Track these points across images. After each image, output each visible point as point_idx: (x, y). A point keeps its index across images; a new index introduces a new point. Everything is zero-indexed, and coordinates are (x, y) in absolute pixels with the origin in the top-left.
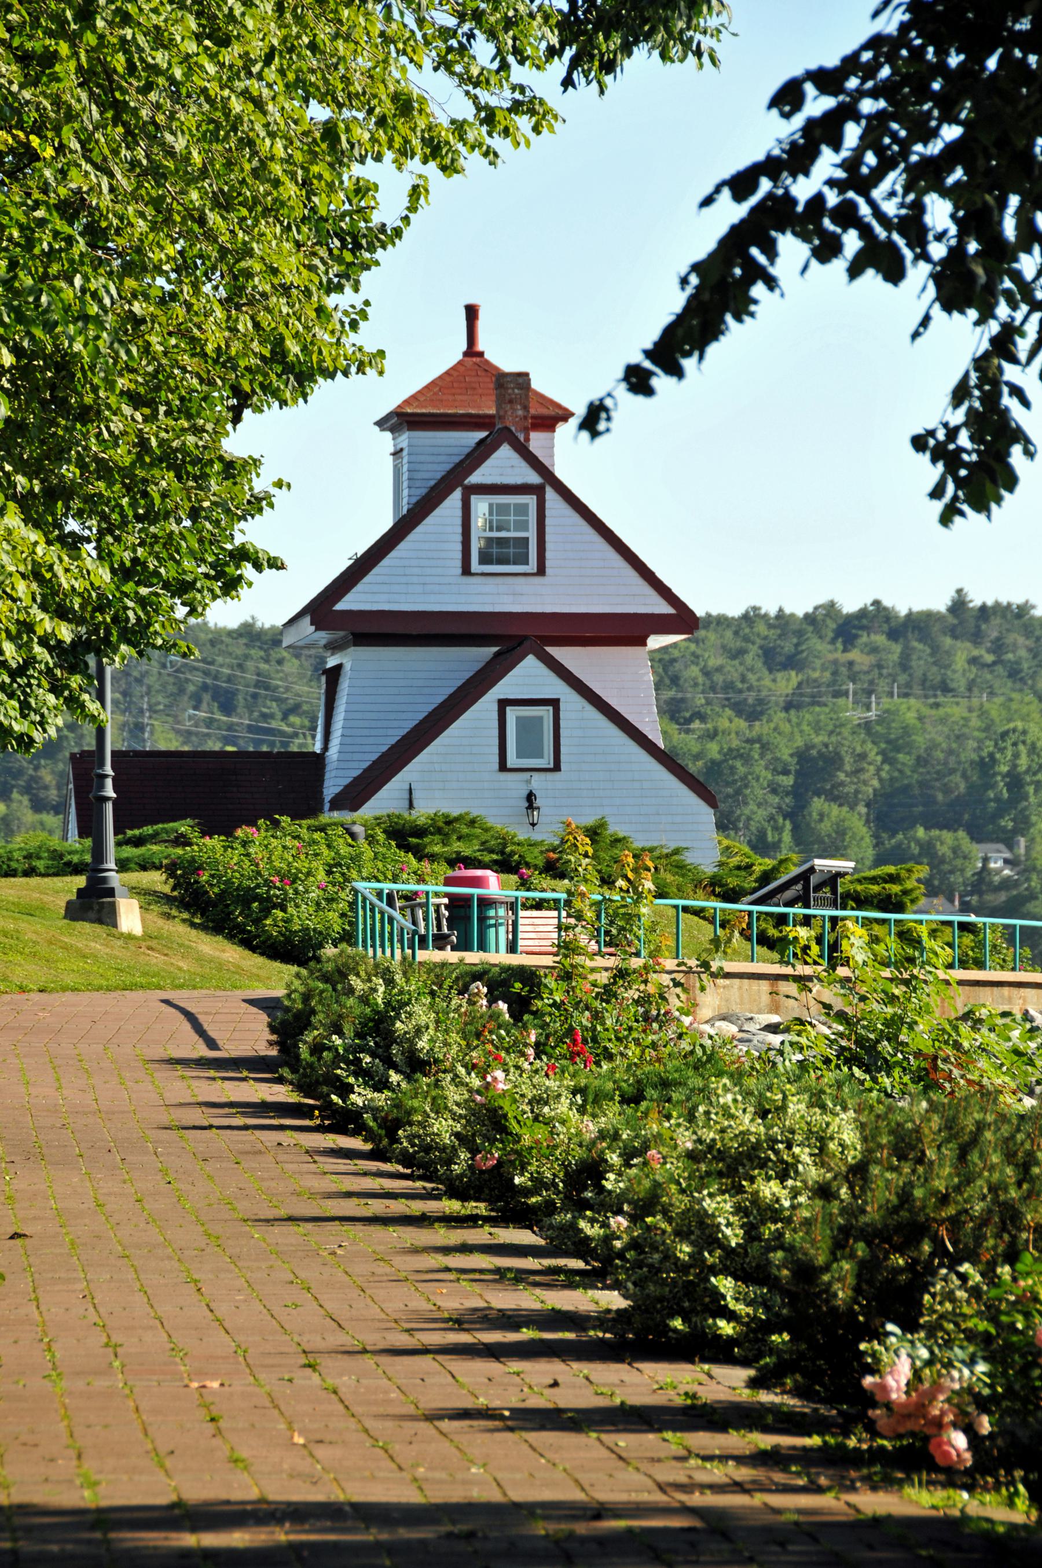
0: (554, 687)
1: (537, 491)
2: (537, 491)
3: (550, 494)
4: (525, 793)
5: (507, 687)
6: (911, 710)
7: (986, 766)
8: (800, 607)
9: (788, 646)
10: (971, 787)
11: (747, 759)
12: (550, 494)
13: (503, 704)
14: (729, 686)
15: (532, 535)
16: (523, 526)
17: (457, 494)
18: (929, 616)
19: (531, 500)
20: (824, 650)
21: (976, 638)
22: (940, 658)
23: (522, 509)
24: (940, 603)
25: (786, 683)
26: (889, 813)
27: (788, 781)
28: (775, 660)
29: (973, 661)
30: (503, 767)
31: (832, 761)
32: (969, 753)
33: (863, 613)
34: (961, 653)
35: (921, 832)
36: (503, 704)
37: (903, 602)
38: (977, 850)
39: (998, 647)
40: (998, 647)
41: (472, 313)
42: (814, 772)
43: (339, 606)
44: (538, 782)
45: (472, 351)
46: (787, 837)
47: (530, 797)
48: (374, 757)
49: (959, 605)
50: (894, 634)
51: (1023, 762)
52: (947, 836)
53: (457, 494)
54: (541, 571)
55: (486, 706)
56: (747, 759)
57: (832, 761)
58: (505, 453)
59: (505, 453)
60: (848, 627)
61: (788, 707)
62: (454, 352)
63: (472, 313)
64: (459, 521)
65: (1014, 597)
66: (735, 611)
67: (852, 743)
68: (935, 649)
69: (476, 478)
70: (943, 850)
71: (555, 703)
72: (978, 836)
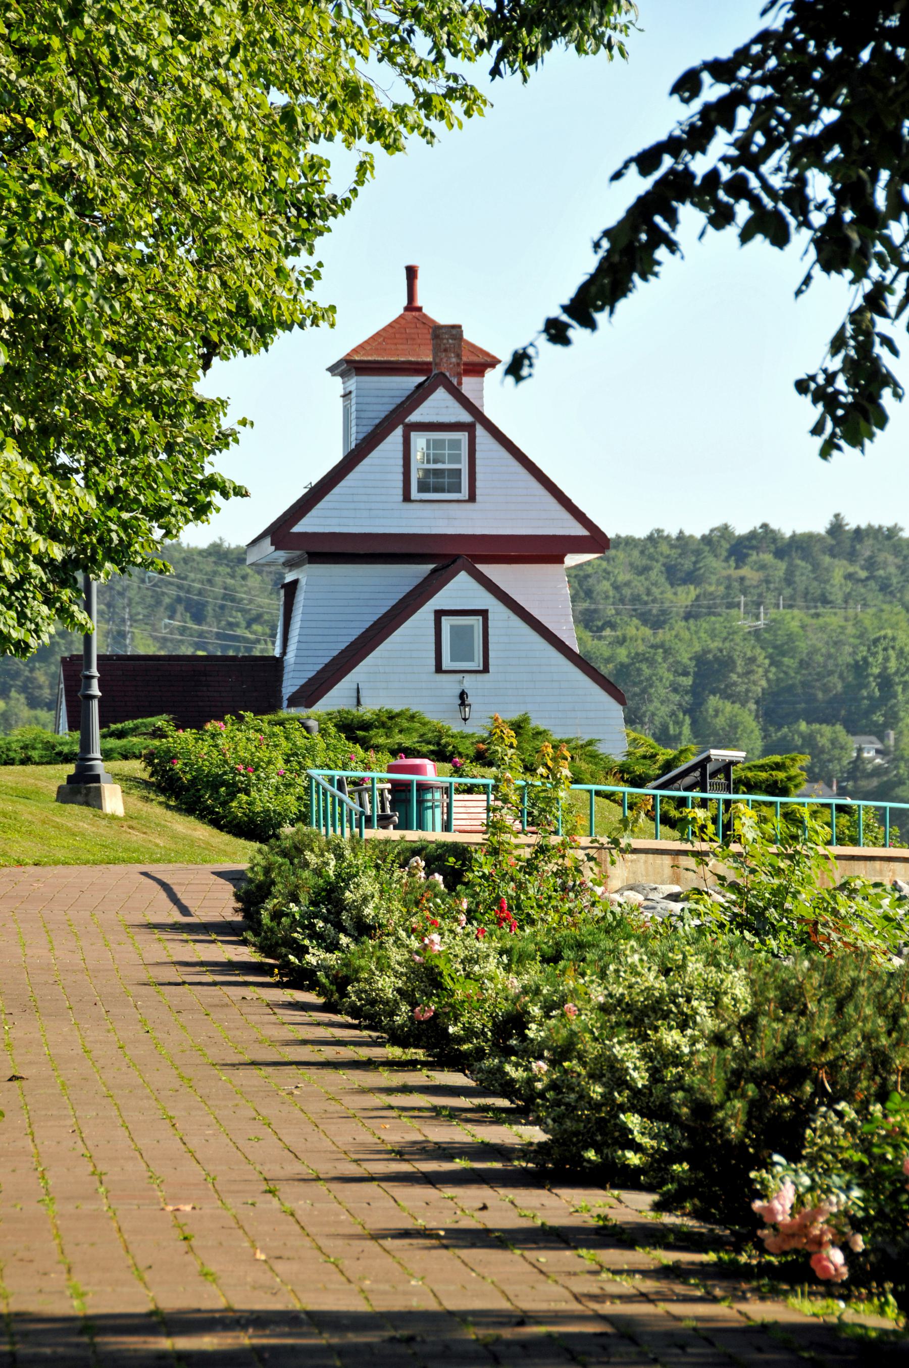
0: (483, 599)
1: (469, 428)
2: (469, 428)
3: (480, 431)
4: (458, 692)
5: (442, 599)
6: (794, 620)
7: (860, 668)
8: (697, 529)
9: (687, 564)
10: (847, 687)
11: (651, 662)
12: (480, 431)
13: (439, 614)
14: (636, 599)
15: (464, 466)
16: (456, 459)
17: (399, 431)
18: (810, 538)
19: (463, 437)
20: (719, 567)
21: (852, 556)
22: (820, 574)
23: (456, 444)
24: (820, 526)
25: (686, 596)
26: (775, 710)
27: (687, 681)
28: (676, 576)
29: (849, 577)
30: (439, 669)
31: (726, 664)
32: (845, 657)
33: (753, 535)
34: (839, 569)
35: (803, 726)
36: (439, 614)
37: (788, 525)
38: (853, 742)
39: (871, 564)
40: (871, 564)
41: (411, 273)
42: (710, 674)
43: (296, 529)
44: (470, 683)
45: (411, 307)
46: (686, 730)
47: (463, 695)
48: (327, 660)
49: (836, 528)
50: (780, 553)
51: (893, 665)
52: (826, 729)
53: (399, 431)
54: (472, 498)
55: (424, 616)
56: (651, 662)
57: (726, 664)
58: (440, 395)
59: (440, 395)
60: (740, 548)
61: (687, 617)
62: (396, 307)
63: (411, 273)
64: (400, 455)
65: (884, 521)
66: (641, 533)
67: (744, 649)
68: (816, 566)
69: (415, 417)
70: (823, 741)
71: (484, 613)
72: (853, 729)
